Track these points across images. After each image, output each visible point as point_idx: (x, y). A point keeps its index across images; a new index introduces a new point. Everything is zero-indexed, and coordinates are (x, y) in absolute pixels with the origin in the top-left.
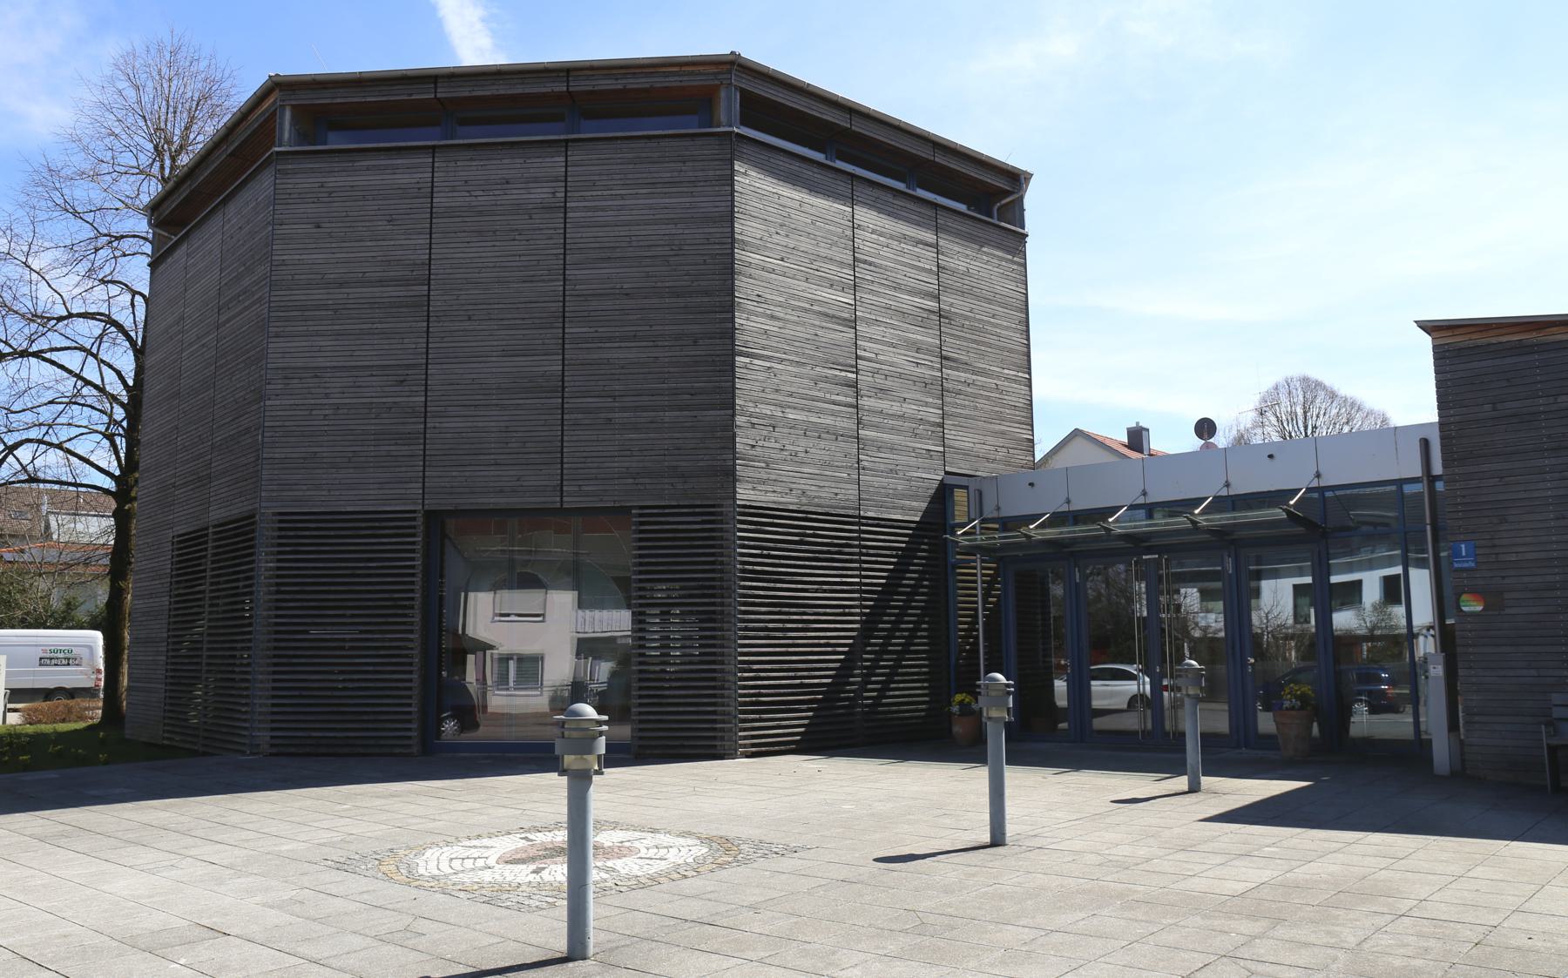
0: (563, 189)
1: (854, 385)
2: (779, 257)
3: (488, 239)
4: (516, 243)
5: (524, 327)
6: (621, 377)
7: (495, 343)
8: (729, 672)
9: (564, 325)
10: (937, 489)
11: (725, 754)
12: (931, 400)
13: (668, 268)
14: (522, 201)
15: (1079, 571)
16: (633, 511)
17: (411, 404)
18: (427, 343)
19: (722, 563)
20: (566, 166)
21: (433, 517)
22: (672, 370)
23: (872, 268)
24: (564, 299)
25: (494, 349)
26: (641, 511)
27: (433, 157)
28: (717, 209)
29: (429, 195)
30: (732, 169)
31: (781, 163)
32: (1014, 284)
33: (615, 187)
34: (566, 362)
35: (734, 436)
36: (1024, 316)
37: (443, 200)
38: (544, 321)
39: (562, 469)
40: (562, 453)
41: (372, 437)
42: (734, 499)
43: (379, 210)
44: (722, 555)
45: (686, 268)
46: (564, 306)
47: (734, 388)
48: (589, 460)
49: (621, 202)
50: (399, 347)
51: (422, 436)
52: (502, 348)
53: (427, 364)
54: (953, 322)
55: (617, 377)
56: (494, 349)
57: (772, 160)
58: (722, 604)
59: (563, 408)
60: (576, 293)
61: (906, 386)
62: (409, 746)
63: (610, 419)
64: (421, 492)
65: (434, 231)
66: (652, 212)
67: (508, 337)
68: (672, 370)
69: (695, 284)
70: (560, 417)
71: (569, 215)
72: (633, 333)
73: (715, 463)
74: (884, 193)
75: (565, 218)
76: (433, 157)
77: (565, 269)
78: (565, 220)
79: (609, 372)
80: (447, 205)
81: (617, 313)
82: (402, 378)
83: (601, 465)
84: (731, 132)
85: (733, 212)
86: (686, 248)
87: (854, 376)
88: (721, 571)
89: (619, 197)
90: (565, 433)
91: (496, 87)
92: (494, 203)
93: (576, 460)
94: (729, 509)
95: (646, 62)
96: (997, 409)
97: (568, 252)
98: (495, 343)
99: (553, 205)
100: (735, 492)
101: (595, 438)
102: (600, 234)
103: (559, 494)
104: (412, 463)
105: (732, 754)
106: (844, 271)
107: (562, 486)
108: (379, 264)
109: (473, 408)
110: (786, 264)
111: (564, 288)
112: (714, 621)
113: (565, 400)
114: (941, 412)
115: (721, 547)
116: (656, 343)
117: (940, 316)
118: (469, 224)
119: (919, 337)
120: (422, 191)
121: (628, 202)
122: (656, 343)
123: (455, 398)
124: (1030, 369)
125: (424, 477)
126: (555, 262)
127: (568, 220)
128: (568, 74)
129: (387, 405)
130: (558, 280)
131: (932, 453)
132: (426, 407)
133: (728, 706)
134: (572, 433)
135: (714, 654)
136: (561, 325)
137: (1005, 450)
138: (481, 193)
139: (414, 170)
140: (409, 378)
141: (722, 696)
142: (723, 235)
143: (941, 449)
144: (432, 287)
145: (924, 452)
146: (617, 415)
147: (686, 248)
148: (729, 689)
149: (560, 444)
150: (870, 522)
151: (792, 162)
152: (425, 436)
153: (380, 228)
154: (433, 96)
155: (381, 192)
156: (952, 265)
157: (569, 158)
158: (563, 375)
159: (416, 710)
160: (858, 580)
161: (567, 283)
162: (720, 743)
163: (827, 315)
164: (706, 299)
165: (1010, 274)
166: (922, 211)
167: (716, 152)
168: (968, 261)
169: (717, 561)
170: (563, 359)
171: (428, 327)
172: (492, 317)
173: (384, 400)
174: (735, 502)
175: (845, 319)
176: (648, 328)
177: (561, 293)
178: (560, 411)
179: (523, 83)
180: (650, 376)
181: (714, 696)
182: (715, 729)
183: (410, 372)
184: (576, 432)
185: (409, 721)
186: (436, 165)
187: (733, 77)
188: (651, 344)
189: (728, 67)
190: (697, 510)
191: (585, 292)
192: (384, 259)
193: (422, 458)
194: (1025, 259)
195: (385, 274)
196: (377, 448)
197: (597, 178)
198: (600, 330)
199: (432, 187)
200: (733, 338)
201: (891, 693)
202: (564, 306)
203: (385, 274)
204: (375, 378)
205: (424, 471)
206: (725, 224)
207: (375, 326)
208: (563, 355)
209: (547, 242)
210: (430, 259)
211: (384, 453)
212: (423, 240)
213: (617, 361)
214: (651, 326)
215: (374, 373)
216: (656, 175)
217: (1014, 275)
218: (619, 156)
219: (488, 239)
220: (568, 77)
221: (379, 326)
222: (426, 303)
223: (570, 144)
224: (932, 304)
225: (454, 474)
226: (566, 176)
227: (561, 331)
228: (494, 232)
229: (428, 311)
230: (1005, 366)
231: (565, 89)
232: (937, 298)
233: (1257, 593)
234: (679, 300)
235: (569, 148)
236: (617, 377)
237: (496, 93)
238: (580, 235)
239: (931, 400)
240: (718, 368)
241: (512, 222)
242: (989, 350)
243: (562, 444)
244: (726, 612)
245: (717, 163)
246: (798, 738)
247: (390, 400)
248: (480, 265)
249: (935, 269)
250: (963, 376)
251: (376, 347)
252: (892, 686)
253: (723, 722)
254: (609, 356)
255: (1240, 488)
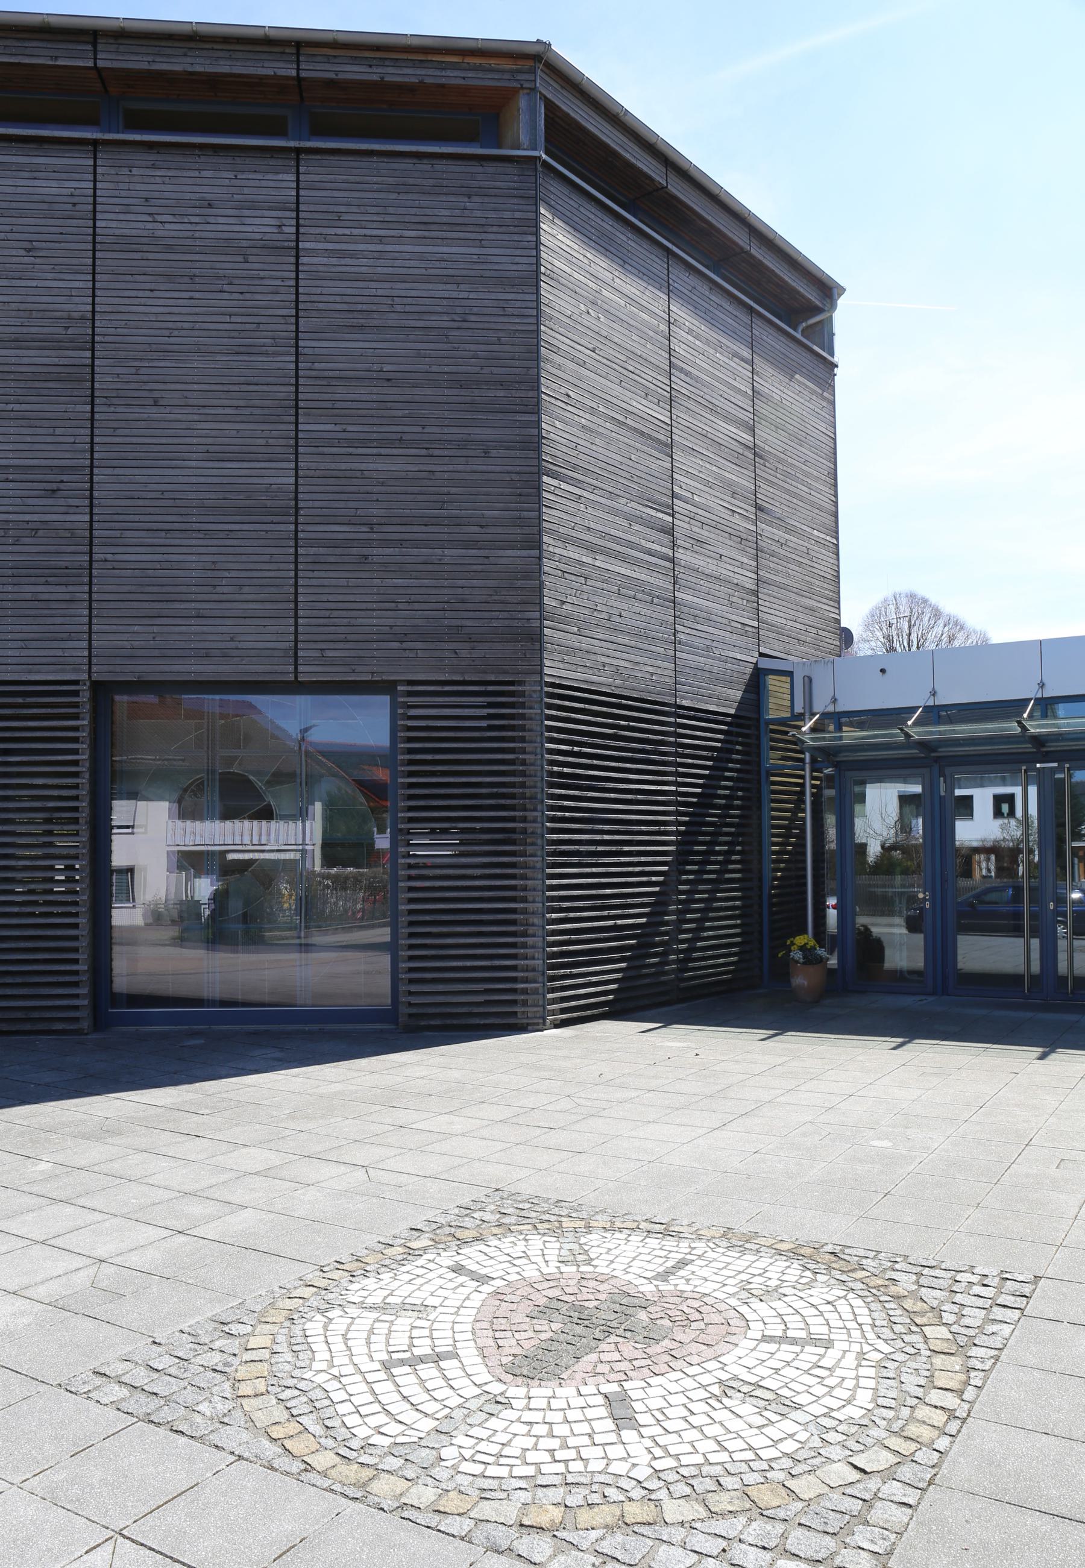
0: (294, 222)
1: (670, 531)
2: (591, 346)
3: (183, 287)
4: (225, 296)
5: (238, 419)
6: (381, 497)
7: (195, 440)
8: (533, 913)
9: (297, 419)
10: (752, 675)
11: (528, 1024)
12: (745, 560)
13: (446, 346)
14: (232, 235)
15: (945, 782)
16: (399, 688)
17: (68, 525)
18: (92, 436)
19: (523, 763)
20: (298, 189)
21: (102, 691)
22: (453, 490)
23: (688, 379)
24: (297, 381)
25: (194, 449)
26: (410, 688)
27: (95, 159)
28: (515, 267)
29: (90, 216)
30: (537, 213)
31: (592, 217)
32: (824, 425)
33: (369, 225)
34: (301, 473)
35: (541, 587)
36: (832, 466)
37: (114, 224)
38: (266, 411)
39: (296, 625)
40: (296, 602)
41: (10, 572)
42: (541, 673)
43: (12, 232)
44: (523, 751)
45: (473, 347)
46: (297, 392)
47: (540, 519)
48: (336, 614)
49: (379, 247)
50: (49, 439)
51: (86, 572)
52: (204, 448)
53: (92, 467)
54: (767, 464)
55: (375, 497)
56: (194, 449)
57: (582, 209)
58: (524, 820)
59: (296, 539)
60: (314, 373)
61: (721, 539)
62: (76, 1020)
63: (366, 557)
64: (86, 653)
65: (98, 269)
66: (423, 264)
67: (213, 433)
68: (453, 490)
69: (486, 370)
70: (292, 550)
71: (302, 260)
72: (399, 436)
73: (515, 623)
74: (701, 284)
75: (297, 264)
76: (95, 159)
77: (297, 339)
78: (297, 267)
79: (363, 489)
80: (118, 232)
81: (375, 405)
82: (54, 486)
83: (353, 621)
84: (535, 158)
85: (537, 272)
86: (473, 318)
87: (670, 519)
88: (523, 774)
89: (376, 240)
90: (300, 574)
91: (189, 60)
92: (190, 234)
93: (315, 613)
94: (534, 688)
95: (415, 42)
96: (807, 578)
97: (301, 314)
98: (195, 440)
99: (279, 244)
100: (542, 665)
101: (343, 582)
102: (349, 291)
103: (292, 660)
104: (72, 612)
105: (538, 1024)
106: (659, 377)
107: (296, 649)
108: (14, 314)
109: (163, 534)
110: (598, 357)
111: (297, 366)
112: (513, 842)
113: (300, 527)
114: (755, 576)
115: (522, 740)
116: (431, 452)
117: (755, 454)
118: (152, 263)
119: (734, 477)
120: (78, 207)
121: (389, 248)
122: (431, 452)
123: (137, 518)
124: (837, 532)
125: (90, 633)
126: (284, 328)
127: (301, 268)
128: (298, 50)
129: (30, 526)
130: (288, 354)
131: (747, 628)
132: (91, 529)
133: (533, 958)
134: (311, 574)
135: (513, 888)
136: (293, 419)
137: (814, 631)
138: (170, 218)
139: (64, 176)
140: (62, 486)
141: (524, 946)
142: (524, 305)
143: (755, 624)
144: (97, 354)
145: (739, 626)
146: (375, 551)
147: (473, 318)
148: (534, 936)
149: (292, 590)
150: (686, 712)
151: (605, 218)
152: (91, 573)
153: (14, 260)
154: (91, 64)
155: (14, 205)
156: (767, 391)
157: (302, 177)
158: (296, 492)
159: (86, 968)
160: (673, 788)
161: (301, 358)
162: (523, 1009)
163: (642, 433)
164: (501, 393)
165: (820, 411)
166: (738, 314)
167: (516, 185)
168: (782, 388)
169: (518, 759)
170: (297, 469)
171: (93, 412)
172: (191, 402)
173: (27, 517)
174: (542, 678)
175: (658, 441)
176: (419, 429)
177: (293, 373)
178: (292, 543)
179: (230, 58)
180: (420, 497)
181: (513, 945)
182: (514, 991)
183: (65, 478)
184: (316, 574)
185: (76, 984)
186: (99, 170)
187: (538, 81)
188: (424, 452)
189: (531, 63)
190: (490, 688)
191: (326, 374)
192: (23, 306)
193: (86, 604)
194: (834, 396)
195: (25, 330)
196: (16, 589)
197: (343, 209)
198: (350, 428)
199: (95, 204)
200: (538, 450)
201: (706, 934)
202: (297, 392)
203: (25, 330)
204: (11, 485)
205: (90, 624)
206: (526, 289)
207: (10, 407)
208: (297, 462)
209: (270, 297)
210: (93, 312)
211: (28, 596)
212: (82, 283)
213: (375, 475)
214: (424, 427)
215: (11, 477)
216: (429, 212)
217: (824, 414)
218: (375, 179)
219: (183, 287)
220: (298, 54)
221: (17, 407)
222: (89, 377)
223: (302, 156)
224: (747, 438)
225: (136, 628)
226: (298, 203)
227: (293, 427)
228: (192, 277)
229: (93, 388)
230: (815, 526)
231: (294, 73)
232: (752, 431)
233: (862, 799)
234: (463, 392)
235: (302, 163)
236: (375, 497)
237: (190, 69)
238: (319, 290)
239: (745, 560)
240: (518, 491)
241: (218, 265)
242: (801, 504)
243: (296, 590)
244: (529, 831)
245: (515, 201)
246: (611, 997)
247: (35, 517)
248: (170, 325)
249: (750, 392)
250: (780, 534)
251: (12, 438)
252: (707, 924)
253: (526, 980)
254: (363, 467)
255: (949, 697)
